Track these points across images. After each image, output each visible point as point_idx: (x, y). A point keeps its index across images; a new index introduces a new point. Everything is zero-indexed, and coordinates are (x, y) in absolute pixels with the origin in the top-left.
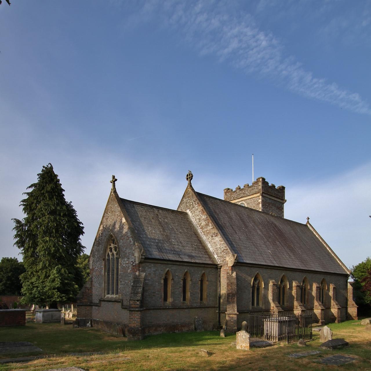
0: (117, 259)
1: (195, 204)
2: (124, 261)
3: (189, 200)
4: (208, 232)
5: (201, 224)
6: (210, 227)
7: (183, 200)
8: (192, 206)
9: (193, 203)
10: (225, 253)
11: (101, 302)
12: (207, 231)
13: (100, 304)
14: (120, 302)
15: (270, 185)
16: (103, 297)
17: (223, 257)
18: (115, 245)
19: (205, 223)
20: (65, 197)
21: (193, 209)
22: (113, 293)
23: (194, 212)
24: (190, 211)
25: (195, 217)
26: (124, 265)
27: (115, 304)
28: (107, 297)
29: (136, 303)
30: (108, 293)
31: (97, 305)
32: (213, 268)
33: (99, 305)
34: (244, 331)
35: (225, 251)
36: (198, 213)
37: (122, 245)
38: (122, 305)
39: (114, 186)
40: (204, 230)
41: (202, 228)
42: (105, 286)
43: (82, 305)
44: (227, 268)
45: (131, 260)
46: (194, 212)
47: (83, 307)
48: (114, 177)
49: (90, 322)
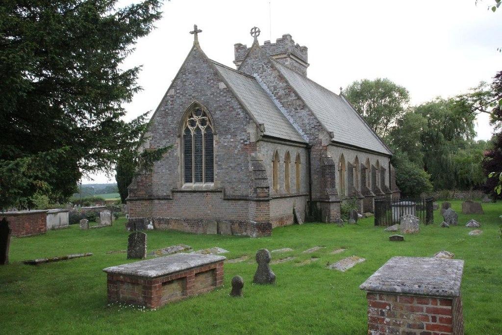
0: (209, 137)
1: (267, 67)
2: (224, 138)
3: (257, 61)
4: (289, 103)
5: (277, 93)
6: (292, 97)
7: (247, 61)
8: (261, 69)
9: (263, 66)
10: (316, 130)
11: (174, 193)
12: (287, 102)
13: (173, 196)
14: (221, 192)
15: (295, 44)
16: (178, 186)
17: (313, 135)
18: (203, 117)
19: (283, 92)
20: (418, 106)
21: (264, 73)
22: (199, 180)
23: (266, 77)
24: (258, 75)
25: (268, 84)
26: (226, 144)
27: (207, 194)
28: (185, 186)
29: (264, 191)
30: (188, 180)
31: (166, 198)
32: (300, 147)
33: (171, 197)
34: (9, 226)
35: (316, 127)
36: (272, 79)
37: (220, 118)
38: (225, 195)
39: (196, 38)
40: (282, 101)
41: (279, 98)
42: (181, 172)
43: (136, 200)
44: (321, 148)
45: (239, 138)
46: (266, 77)
47: (138, 202)
48: (196, 27)
49: (151, 222)
